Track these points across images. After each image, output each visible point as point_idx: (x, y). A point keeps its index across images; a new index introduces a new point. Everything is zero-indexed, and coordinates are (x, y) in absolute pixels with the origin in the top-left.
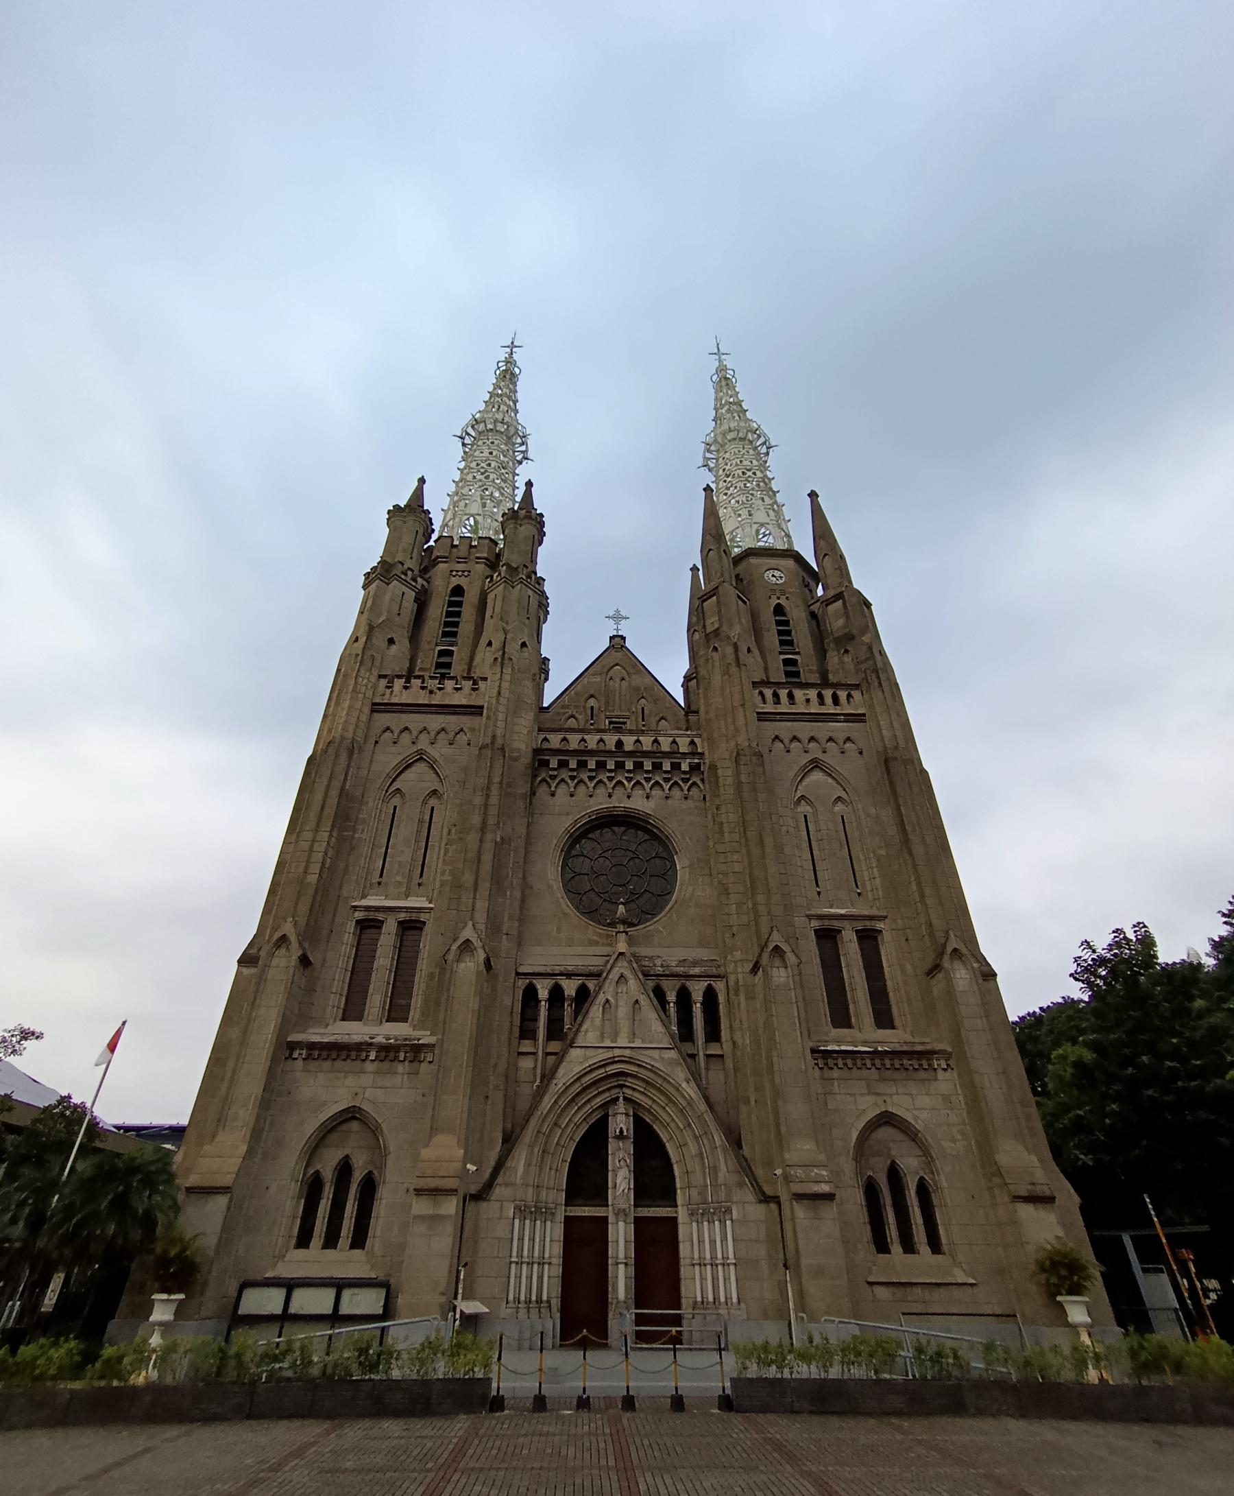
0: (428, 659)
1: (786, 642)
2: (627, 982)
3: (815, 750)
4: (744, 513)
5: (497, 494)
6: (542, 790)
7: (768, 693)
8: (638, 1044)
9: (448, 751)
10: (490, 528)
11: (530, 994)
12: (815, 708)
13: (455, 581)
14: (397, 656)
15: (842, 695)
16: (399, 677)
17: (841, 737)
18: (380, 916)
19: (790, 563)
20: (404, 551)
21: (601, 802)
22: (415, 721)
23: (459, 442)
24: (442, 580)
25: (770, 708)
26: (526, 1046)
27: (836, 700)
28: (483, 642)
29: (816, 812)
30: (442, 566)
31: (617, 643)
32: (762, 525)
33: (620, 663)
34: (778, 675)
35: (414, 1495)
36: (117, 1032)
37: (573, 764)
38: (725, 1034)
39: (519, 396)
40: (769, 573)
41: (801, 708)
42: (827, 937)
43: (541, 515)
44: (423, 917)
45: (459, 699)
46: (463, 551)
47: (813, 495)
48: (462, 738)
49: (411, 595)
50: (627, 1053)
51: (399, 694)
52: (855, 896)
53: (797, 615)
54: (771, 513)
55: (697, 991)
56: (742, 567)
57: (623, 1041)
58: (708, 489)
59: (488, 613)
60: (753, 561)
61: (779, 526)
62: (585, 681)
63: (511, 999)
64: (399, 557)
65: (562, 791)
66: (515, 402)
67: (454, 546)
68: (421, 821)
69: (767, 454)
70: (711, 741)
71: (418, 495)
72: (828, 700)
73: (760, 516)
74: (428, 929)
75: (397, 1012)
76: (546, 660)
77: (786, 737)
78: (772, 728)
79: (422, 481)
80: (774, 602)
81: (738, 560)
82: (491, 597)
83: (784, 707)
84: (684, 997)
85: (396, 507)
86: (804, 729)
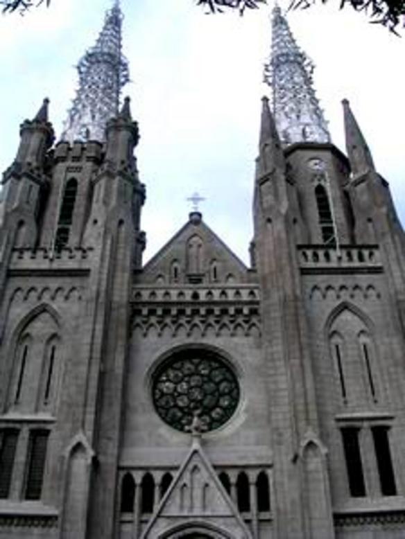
0: (49, 238)
1: (325, 213)
2: (199, 470)
3: (345, 297)
4: (293, 116)
5: (105, 109)
6: (138, 333)
7: (309, 253)
8: (208, 513)
9: (64, 305)
10: (97, 134)
11: (129, 480)
12: (345, 264)
13: (71, 175)
14: (26, 235)
15: (366, 253)
16: (28, 249)
17: (364, 285)
18: (18, 426)
19: (327, 155)
20: (32, 154)
21: (182, 339)
22: (39, 283)
23: (76, 71)
24: (60, 175)
25: (311, 264)
26: (127, 517)
27: (361, 258)
28: (90, 221)
29: (344, 343)
30: (61, 167)
31: (196, 219)
32: (307, 125)
33: (200, 234)
34: (318, 239)
35: (149, 538)
36: (347, 128)
37: (159, 312)
38: (272, 505)
39: (123, 35)
40: (312, 163)
41: (334, 264)
42: (350, 435)
43: (136, 123)
44: (49, 427)
45: (72, 265)
46: (76, 152)
47: (345, 102)
48: (76, 294)
49: (36, 188)
50: (200, 520)
51: (27, 262)
52: (371, 402)
53: (332, 193)
54: (314, 116)
55: (253, 476)
56: (291, 158)
57: (197, 511)
58: (265, 99)
59: (95, 199)
60: (299, 153)
61: (319, 125)
62: (172, 247)
63: (111, 483)
64: (29, 159)
65: (153, 334)
66: (120, 39)
67: (69, 149)
68: (45, 357)
69: (312, 72)
70: (267, 293)
71: (44, 112)
72: (355, 257)
73: (306, 118)
74: (52, 436)
75: (32, 492)
76: (143, 234)
77: (323, 286)
78: (311, 280)
79: (47, 101)
80: (316, 183)
81: (288, 153)
82: (97, 187)
83: (322, 263)
84: (243, 479)
85: (27, 122)
86: (338, 280)
